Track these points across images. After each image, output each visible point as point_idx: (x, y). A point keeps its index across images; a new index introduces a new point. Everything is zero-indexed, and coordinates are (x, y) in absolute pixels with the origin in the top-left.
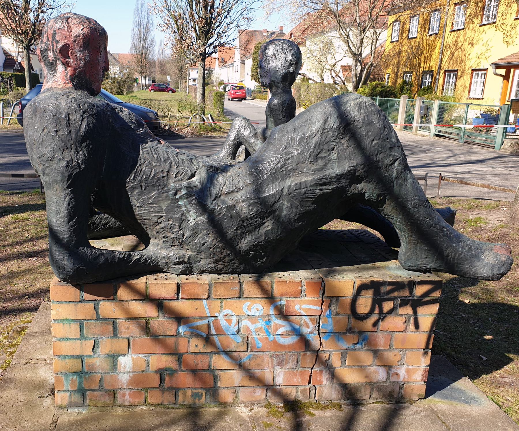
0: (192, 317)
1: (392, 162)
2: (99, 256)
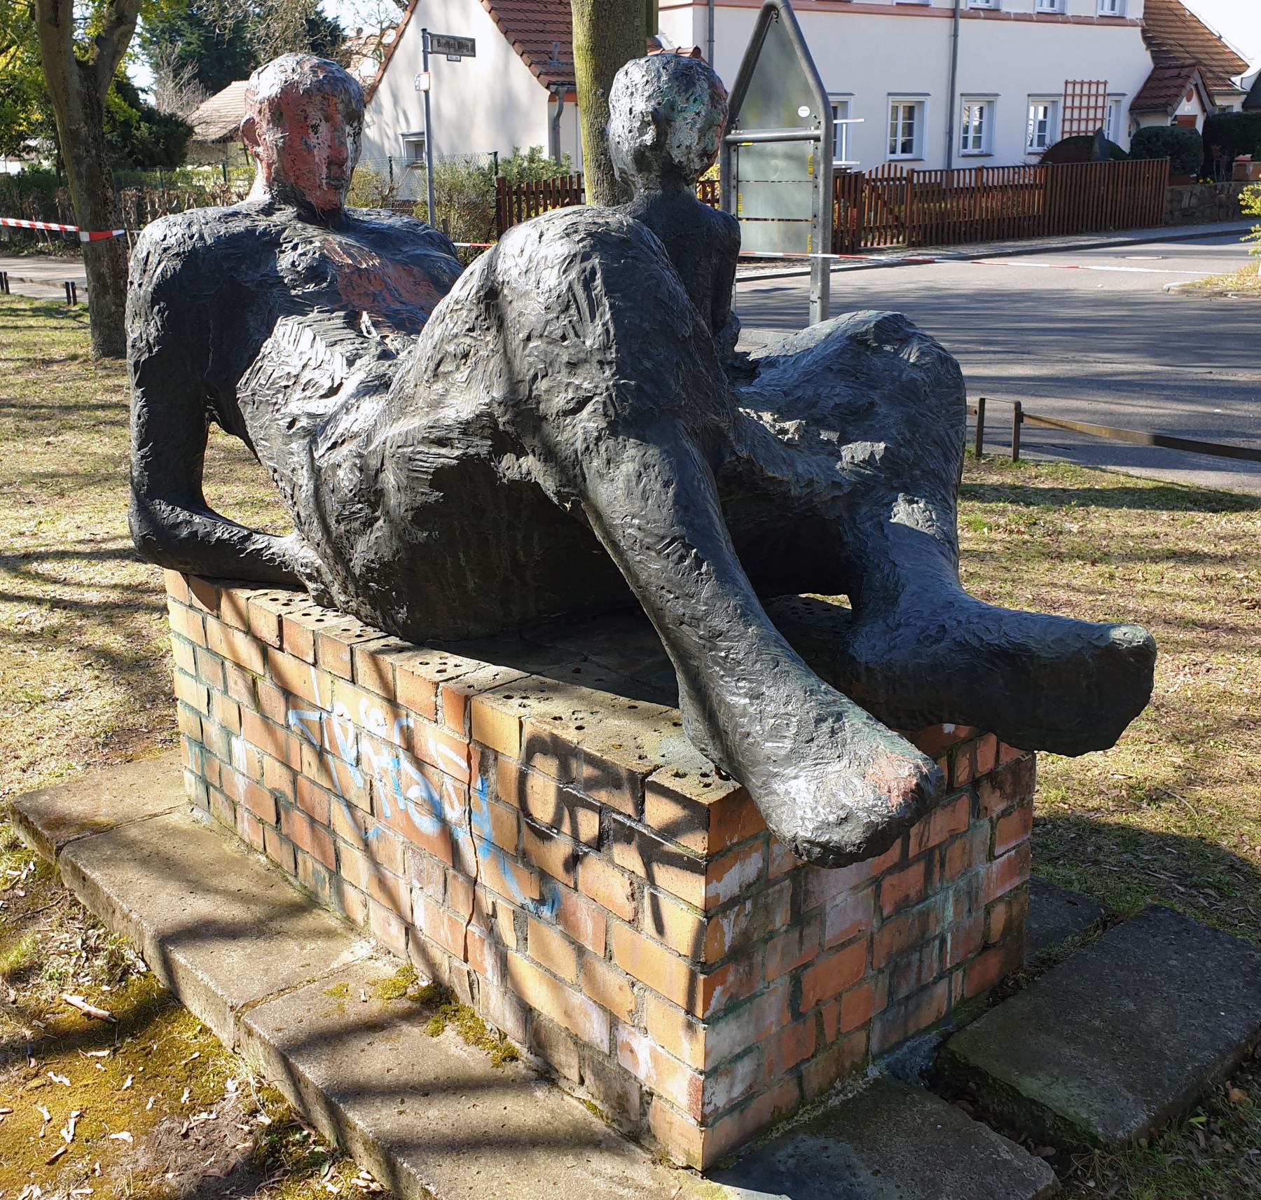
0: (302, 699)
1: (572, 405)
2: (181, 523)
